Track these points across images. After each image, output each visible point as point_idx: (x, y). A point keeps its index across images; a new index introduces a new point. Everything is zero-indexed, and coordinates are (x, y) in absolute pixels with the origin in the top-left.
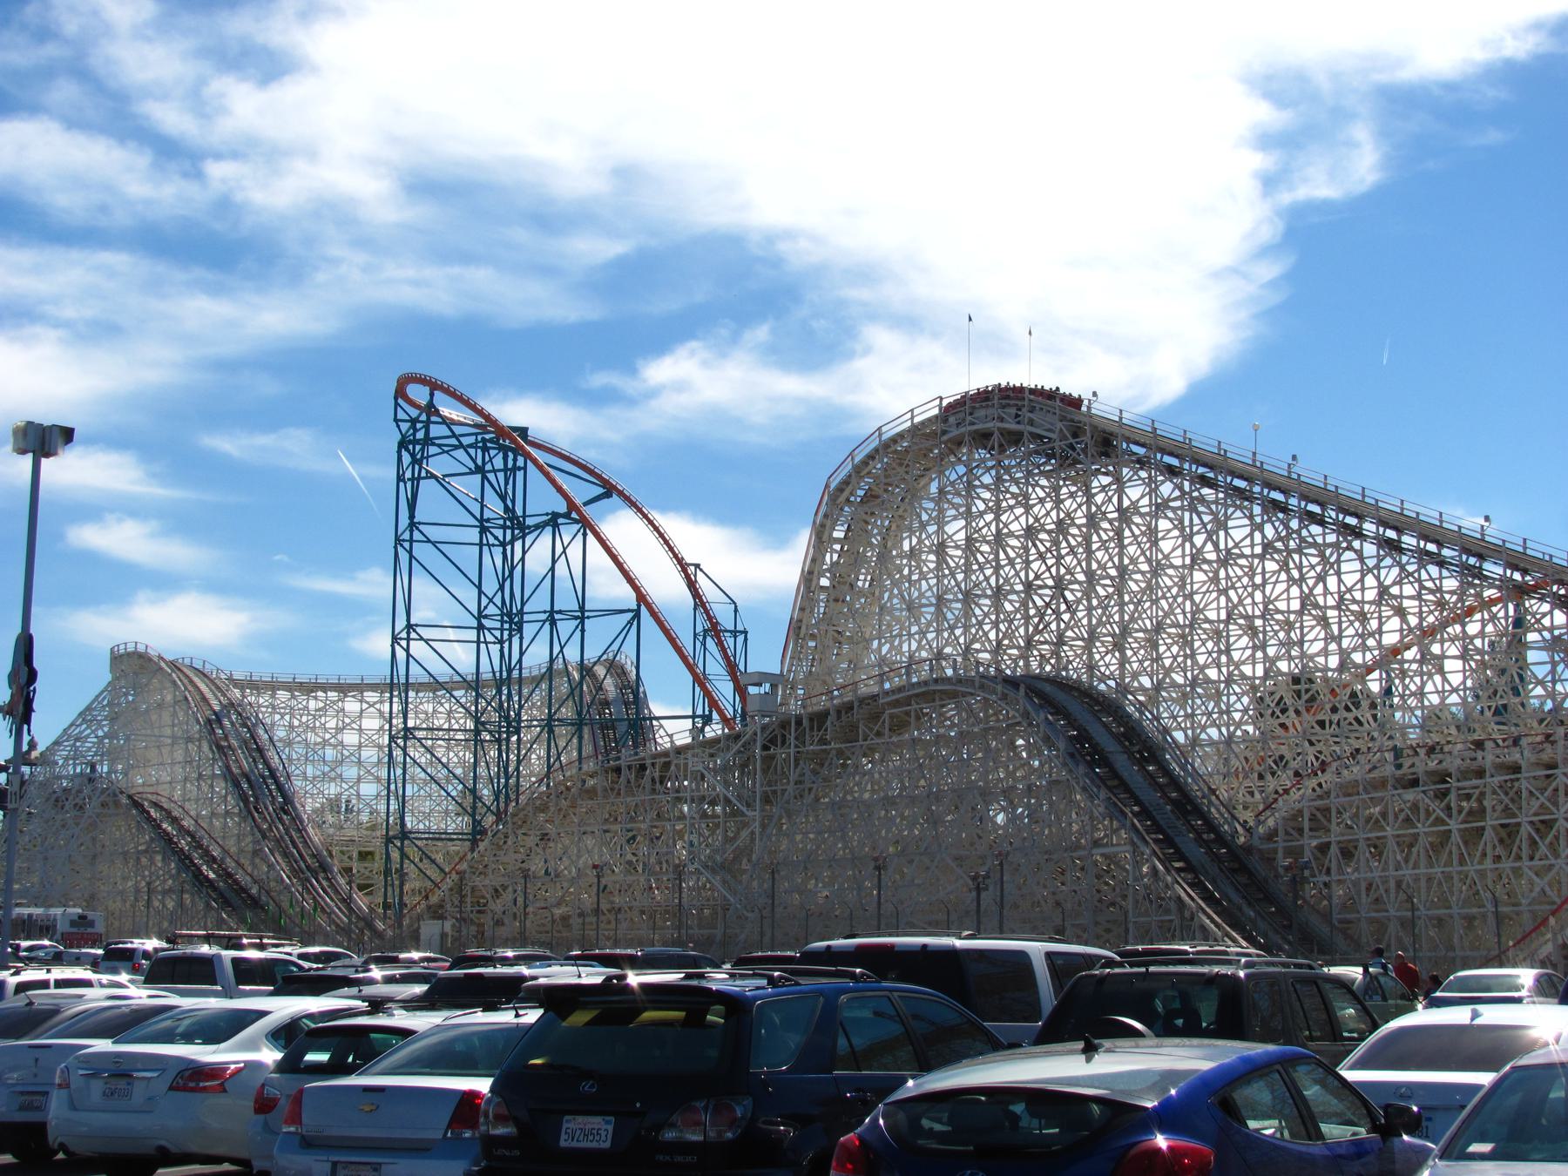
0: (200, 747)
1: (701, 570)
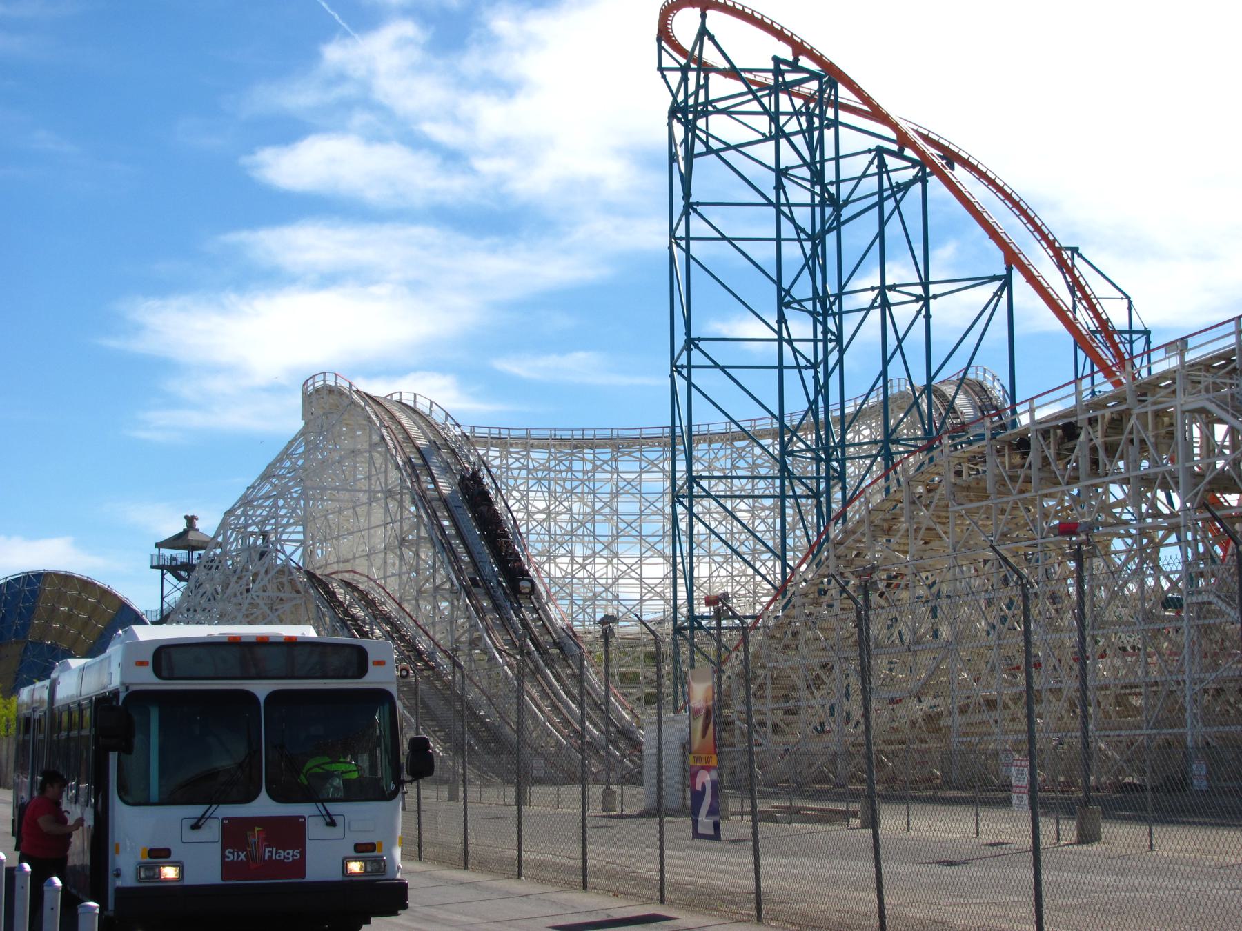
0: (401, 503)
1: (1080, 256)
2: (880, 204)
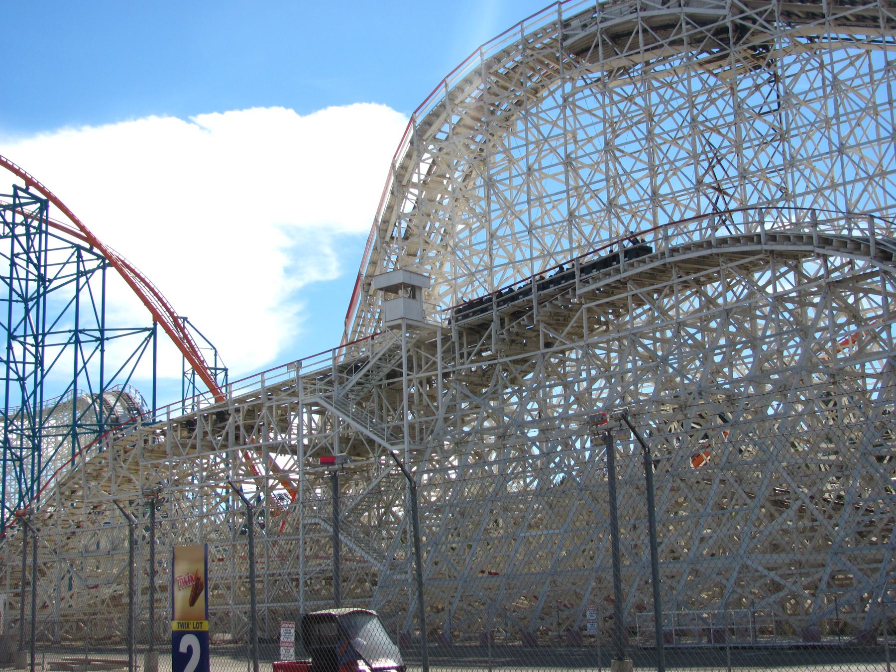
1: (188, 322)
2: (77, 279)
